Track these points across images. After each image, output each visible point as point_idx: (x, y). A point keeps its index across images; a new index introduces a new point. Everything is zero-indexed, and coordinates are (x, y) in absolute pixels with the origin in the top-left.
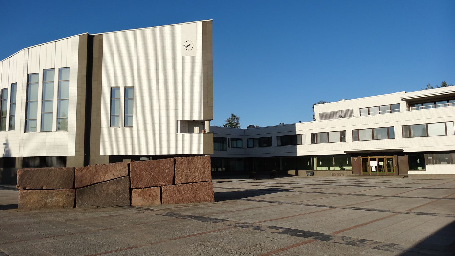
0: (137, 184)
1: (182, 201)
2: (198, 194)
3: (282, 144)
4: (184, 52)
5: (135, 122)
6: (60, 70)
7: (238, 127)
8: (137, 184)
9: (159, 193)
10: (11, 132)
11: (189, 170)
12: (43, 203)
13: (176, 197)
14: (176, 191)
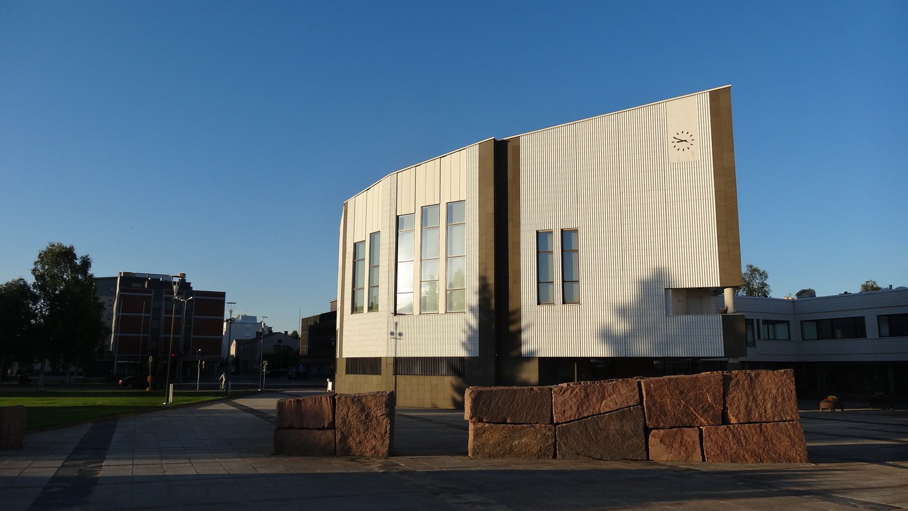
0: (657, 422)
1: (744, 457)
2: (774, 445)
3: (893, 333)
4: (674, 155)
5: (582, 294)
6: (449, 206)
7: (765, 294)
8: (657, 422)
9: (697, 439)
10: (373, 314)
11: (751, 398)
12: (507, 447)
13: (731, 449)
14: (731, 438)
